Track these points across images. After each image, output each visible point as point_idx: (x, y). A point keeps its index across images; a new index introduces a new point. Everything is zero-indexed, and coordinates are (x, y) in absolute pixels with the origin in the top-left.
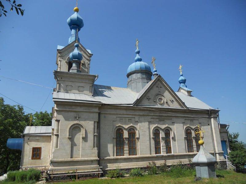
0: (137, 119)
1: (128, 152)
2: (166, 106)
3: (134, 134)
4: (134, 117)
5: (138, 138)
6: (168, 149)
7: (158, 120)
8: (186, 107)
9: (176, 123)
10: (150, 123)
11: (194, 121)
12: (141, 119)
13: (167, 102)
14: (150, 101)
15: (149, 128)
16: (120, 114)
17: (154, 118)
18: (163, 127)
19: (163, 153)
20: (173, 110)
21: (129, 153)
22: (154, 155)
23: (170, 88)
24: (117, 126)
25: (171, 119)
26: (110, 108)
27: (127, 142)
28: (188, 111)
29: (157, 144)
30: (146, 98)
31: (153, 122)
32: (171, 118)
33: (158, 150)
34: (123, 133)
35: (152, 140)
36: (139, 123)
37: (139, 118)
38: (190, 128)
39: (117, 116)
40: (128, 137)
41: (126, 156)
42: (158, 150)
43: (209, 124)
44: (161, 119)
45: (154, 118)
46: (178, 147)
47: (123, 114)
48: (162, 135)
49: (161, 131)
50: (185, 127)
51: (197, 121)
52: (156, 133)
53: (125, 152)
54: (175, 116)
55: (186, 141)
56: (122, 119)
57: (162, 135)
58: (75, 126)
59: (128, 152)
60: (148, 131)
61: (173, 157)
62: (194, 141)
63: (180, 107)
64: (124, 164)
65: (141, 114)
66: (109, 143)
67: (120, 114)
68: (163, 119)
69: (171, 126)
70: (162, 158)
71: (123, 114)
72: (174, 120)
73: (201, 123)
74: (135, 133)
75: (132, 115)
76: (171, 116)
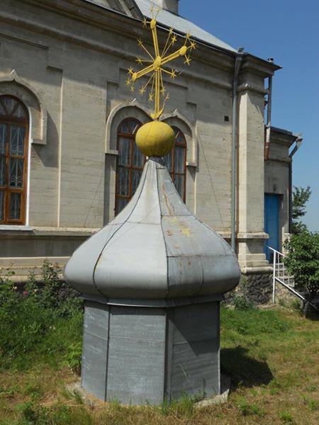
9: (71, 77)
25: (46, 48)
40: (240, 244)
50: (116, 106)
51: (182, 92)
54: (68, 40)
55: (113, 174)
76: (46, 33)
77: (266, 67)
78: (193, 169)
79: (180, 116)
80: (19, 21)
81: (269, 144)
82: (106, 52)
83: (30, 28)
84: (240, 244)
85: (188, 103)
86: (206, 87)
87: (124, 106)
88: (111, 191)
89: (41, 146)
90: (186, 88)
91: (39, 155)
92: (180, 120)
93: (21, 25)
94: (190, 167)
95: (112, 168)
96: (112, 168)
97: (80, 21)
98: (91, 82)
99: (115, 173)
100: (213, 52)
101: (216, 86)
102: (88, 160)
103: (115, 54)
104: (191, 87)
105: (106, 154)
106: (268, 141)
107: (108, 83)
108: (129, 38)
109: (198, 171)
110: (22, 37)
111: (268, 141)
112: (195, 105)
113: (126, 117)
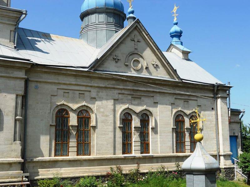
1: (75, 149)
4: (89, 90)
5: (95, 127)
6: (145, 147)
8: (178, 77)
9: (161, 104)
10: (116, 101)
11: (190, 102)
15: (114, 111)
17: (123, 94)
19: (136, 152)
21: (77, 152)
23: (154, 43)
24: (59, 104)
25: (153, 96)
29: (127, 137)
32: (152, 95)
33: (126, 147)
36: (97, 100)
37: (98, 92)
38: (182, 114)
41: (72, 156)
42: (126, 147)
43: (213, 109)
44: (136, 97)
45: (123, 94)
46: (161, 143)
47: (70, 84)
48: (136, 122)
51: (152, 99)
52: (126, 119)
54: (159, 92)
55: (175, 134)
57: (136, 122)
60: (112, 116)
61: (152, 159)
62: (187, 134)
66: (43, 134)
67: (64, 84)
68: (138, 97)
69: (151, 109)
70: (134, 160)
71: (70, 84)
72: (158, 98)
74: (90, 118)
76: (153, 92)
104: (198, 99)
106: (229, 116)
107: (172, 104)
111: (229, 116)
112: (201, 106)
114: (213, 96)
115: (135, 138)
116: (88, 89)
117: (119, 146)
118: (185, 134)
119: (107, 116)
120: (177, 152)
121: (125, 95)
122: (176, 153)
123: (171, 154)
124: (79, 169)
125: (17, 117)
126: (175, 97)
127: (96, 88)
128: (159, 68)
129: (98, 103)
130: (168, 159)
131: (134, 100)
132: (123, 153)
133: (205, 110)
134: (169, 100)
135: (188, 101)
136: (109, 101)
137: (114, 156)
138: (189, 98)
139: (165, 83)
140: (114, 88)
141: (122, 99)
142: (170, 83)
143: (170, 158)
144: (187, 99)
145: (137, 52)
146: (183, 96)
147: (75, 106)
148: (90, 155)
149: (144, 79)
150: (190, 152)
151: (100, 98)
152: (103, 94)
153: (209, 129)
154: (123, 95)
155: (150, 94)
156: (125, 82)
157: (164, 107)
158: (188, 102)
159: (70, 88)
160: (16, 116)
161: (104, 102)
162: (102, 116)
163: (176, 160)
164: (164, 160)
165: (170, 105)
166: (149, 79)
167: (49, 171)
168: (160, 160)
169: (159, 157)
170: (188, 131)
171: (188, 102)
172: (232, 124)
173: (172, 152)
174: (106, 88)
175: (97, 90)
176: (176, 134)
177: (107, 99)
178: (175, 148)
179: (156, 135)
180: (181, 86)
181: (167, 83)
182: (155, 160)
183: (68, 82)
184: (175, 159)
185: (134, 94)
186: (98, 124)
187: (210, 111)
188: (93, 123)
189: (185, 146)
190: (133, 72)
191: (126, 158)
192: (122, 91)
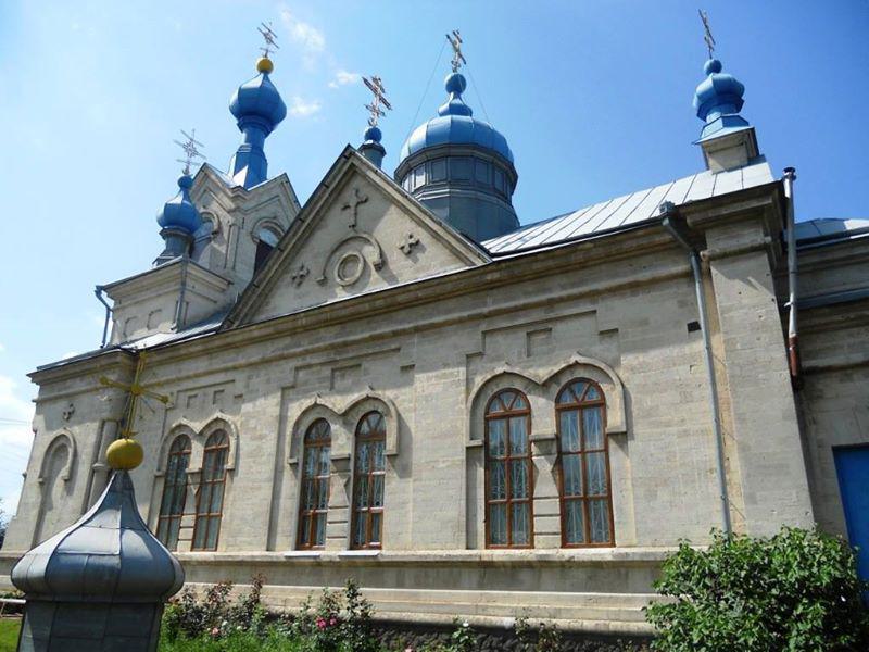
0: (239, 387)
1: (555, 524)
2: (377, 284)
3: (378, 436)
4: (231, 379)
5: (626, 433)
6: (365, 527)
7: (327, 371)
9: (423, 370)
10: (288, 391)
11: (559, 328)
12: (255, 381)
13: (381, 266)
14: (305, 286)
15: (282, 419)
16: (188, 378)
17: (310, 366)
18: (340, 403)
19: (334, 548)
20: (401, 298)
21: (194, 540)
22: (285, 550)
24: (174, 425)
25: (398, 349)
26: (396, 310)
27: (195, 491)
28: (496, 276)
29: (312, 496)
30: (288, 278)
31: (306, 383)
32: (393, 347)
33: (308, 530)
34: (190, 453)
35: (288, 473)
36: (244, 402)
37: (249, 378)
38: (518, 385)
39: (179, 388)
40: (130, 472)
41: (546, 547)
42: (308, 530)
43: (694, 327)
44: (343, 364)
45: (310, 366)
46: (427, 511)
47: (197, 376)
48: (342, 443)
49: (336, 428)
50: (295, 411)
51: (587, 321)
52: (314, 434)
53: (539, 524)
54: (417, 330)
55: (481, 472)
56: (195, 396)
57: (342, 443)
58: (213, 430)
59: (191, 537)
60: (273, 436)
61: (380, 571)
62: (544, 466)
63: (461, 264)
64: (559, 599)
65: (255, 359)
67: (188, 378)
68: (352, 363)
69: (387, 395)
70: (319, 570)
71: (197, 376)
72: (415, 349)
73: (612, 333)
75: (226, 370)
76: (396, 334)
77: (735, 202)
78: (622, 437)
79: (582, 360)
80: (371, 336)
81: (795, 340)
82: (461, 321)
83: (381, 337)
84: (130, 472)
85: (601, 333)
86: (634, 294)
87: (489, 377)
88: (478, 496)
89: (395, 456)
90: (595, 312)
91: (393, 466)
92: (586, 365)
93: (373, 338)
94: (614, 435)
95: (478, 465)
96: (478, 465)
97: (430, 302)
98: (446, 365)
99: (483, 470)
100: (618, 238)
101: (654, 283)
102: (444, 462)
103: (471, 318)
104: (600, 307)
105: (467, 448)
106: (792, 335)
107: (468, 356)
108: (492, 289)
109: (633, 439)
110: (377, 349)
111: (792, 335)
112: (617, 330)
113: (496, 390)
114: (681, 268)
115: (338, 493)
116: (230, 376)
117: (287, 524)
118: (532, 465)
119: (261, 437)
120: (491, 542)
121: (315, 369)
122: (487, 547)
123: (461, 552)
124: (618, 598)
125: (96, 465)
126: (484, 327)
127: (247, 369)
128: (423, 250)
129: (247, 407)
130: (444, 572)
131: (343, 376)
132: (354, 546)
133: (643, 346)
134: (456, 347)
135: (550, 326)
136: (270, 398)
137: (267, 553)
138: (552, 315)
139: (429, 292)
140: (283, 357)
141: (306, 383)
142: (449, 287)
143: (455, 570)
144: (543, 322)
145: (356, 235)
146: (521, 313)
147: (197, 426)
148: (216, 550)
149: (355, 305)
150: (559, 543)
151: (252, 392)
152: (258, 381)
153: (674, 429)
154: (309, 371)
155: (382, 346)
156: (313, 332)
157: (436, 377)
158: (551, 330)
159: (197, 385)
160: (96, 461)
161: (261, 402)
162: (252, 439)
163: (482, 577)
164: (427, 576)
165: (459, 364)
166: (369, 298)
167: (597, 601)
168: (409, 574)
169: (405, 562)
170: (547, 454)
171: (551, 330)
172: (855, 376)
173: (265, 548)
174: (266, 362)
175: (247, 372)
176: (486, 469)
177: (266, 395)
178: (481, 527)
179: (403, 480)
180: (499, 281)
181: (438, 290)
182: (391, 574)
183: (191, 373)
184: (475, 575)
185: (338, 358)
186: (241, 462)
187: (680, 341)
188: (229, 465)
189: (532, 516)
190: (339, 290)
191: (293, 563)
192: (304, 359)
